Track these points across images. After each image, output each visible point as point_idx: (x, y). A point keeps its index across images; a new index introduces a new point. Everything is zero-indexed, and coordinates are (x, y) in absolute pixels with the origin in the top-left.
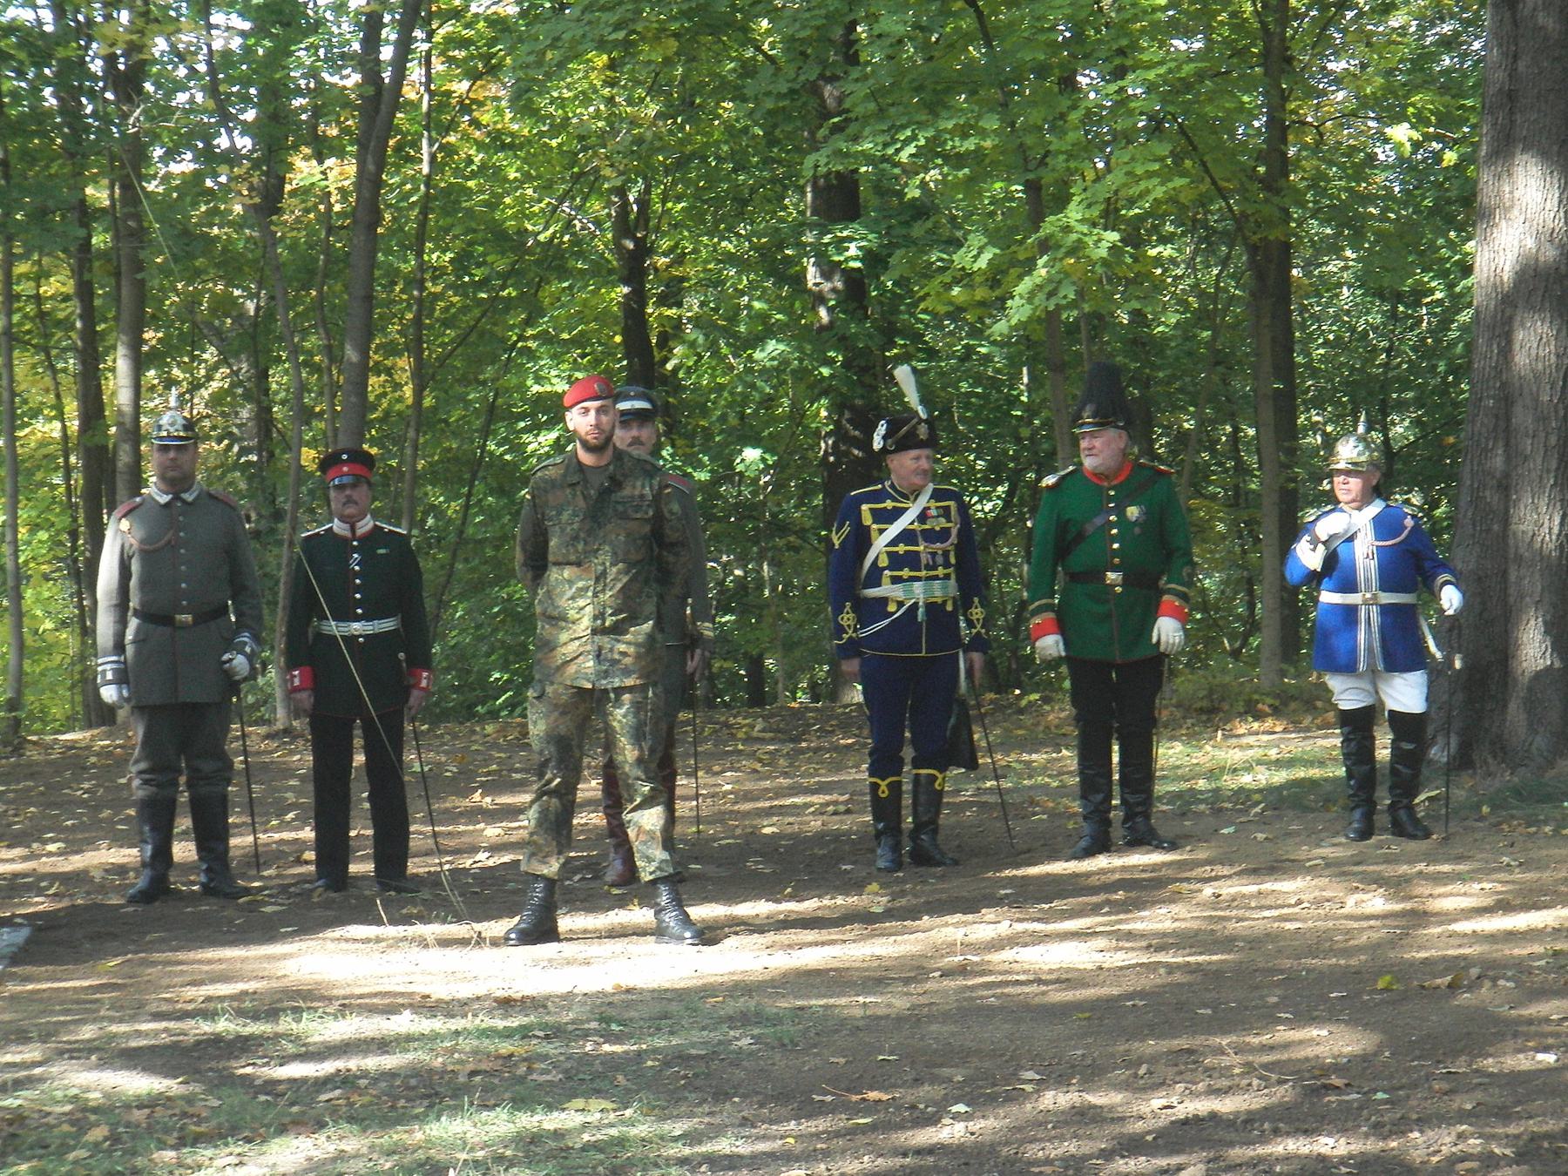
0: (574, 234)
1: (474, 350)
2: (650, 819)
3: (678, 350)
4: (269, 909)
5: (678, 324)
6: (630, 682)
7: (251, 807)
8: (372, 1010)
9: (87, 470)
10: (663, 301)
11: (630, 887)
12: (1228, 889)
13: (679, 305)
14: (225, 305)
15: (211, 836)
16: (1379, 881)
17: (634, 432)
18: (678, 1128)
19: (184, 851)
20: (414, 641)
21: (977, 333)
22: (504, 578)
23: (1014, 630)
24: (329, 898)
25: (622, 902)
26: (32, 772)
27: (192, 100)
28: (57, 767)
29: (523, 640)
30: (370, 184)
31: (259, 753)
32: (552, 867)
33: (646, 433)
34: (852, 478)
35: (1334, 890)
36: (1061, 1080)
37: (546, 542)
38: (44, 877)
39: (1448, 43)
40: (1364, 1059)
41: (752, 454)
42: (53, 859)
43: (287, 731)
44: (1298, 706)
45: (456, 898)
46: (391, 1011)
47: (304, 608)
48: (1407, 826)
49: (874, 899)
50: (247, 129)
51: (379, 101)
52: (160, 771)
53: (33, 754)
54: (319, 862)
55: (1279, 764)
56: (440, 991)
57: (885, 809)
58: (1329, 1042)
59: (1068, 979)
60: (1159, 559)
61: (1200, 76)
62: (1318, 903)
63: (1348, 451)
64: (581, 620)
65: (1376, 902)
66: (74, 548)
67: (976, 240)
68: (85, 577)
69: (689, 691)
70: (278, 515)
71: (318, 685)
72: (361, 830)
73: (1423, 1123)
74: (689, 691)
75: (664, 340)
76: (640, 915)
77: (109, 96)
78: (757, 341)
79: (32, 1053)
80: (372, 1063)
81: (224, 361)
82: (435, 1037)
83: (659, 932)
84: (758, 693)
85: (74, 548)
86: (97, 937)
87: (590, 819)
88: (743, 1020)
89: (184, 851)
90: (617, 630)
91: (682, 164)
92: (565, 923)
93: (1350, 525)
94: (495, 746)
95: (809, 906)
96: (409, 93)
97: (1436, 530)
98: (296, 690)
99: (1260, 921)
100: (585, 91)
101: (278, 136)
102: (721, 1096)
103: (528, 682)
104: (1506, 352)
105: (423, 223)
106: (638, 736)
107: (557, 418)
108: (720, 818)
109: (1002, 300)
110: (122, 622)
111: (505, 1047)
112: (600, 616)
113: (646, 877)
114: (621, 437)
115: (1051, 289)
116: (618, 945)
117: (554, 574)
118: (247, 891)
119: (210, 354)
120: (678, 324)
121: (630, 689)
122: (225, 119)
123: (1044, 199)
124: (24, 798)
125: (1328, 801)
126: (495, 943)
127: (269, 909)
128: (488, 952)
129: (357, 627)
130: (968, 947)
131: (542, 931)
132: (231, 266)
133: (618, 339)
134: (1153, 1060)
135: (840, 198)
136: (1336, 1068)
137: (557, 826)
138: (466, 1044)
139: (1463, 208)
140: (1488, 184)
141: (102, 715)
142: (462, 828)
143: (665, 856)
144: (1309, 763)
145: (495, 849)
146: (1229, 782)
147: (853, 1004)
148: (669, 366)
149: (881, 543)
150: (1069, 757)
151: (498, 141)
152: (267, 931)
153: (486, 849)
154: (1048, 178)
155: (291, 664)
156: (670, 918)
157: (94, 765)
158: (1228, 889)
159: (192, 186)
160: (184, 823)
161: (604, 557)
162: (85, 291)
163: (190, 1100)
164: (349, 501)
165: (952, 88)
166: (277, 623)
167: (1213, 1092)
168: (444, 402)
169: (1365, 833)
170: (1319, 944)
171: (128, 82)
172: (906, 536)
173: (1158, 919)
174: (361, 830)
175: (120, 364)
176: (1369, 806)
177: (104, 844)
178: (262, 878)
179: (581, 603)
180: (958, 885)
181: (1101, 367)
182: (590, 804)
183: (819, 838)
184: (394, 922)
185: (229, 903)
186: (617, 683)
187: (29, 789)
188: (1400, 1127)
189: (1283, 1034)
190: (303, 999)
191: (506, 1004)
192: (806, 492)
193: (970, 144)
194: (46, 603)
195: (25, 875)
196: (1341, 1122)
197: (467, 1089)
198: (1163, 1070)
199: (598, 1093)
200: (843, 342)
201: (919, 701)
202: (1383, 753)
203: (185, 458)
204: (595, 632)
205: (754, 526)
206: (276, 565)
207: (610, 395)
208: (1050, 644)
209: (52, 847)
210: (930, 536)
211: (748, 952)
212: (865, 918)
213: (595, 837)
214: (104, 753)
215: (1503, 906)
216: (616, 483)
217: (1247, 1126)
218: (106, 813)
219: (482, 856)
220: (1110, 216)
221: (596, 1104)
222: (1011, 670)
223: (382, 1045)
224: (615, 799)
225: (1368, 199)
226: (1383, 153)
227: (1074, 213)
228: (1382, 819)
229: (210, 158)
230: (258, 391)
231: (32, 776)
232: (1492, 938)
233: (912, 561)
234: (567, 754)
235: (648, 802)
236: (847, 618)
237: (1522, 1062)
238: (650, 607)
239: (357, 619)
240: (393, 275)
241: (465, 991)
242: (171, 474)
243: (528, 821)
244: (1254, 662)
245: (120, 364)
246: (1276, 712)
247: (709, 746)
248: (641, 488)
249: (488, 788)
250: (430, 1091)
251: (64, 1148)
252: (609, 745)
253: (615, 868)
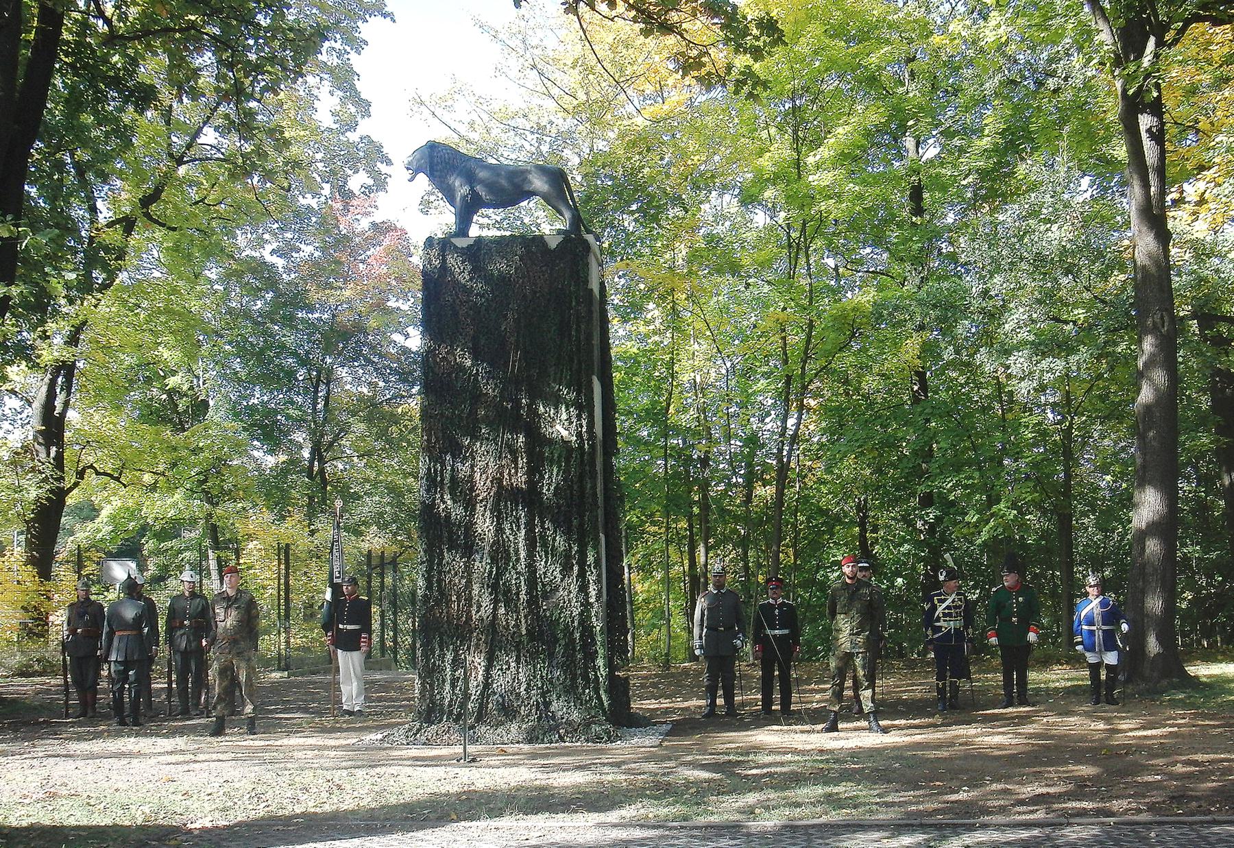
1: (813, 546)
2: (868, 693)
8: (779, 753)
9: (691, 581)
10: (872, 532)
11: (861, 714)
12: (1051, 720)
14: (735, 531)
15: (729, 697)
16: (1102, 718)
18: (876, 792)
19: (720, 701)
21: (971, 543)
22: (823, 616)
23: (981, 634)
24: (766, 717)
26: (673, 675)
29: (828, 638)
30: (780, 493)
32: (836, 708)
33: (867, 574)
34: (932, 585)
35: (1087, 721)
36: (999, 781)
39: (1123, 449)
40: (1098, 776)
41: (900, 580)
44: (1076, 661)
45: (806, 717)
46: (785, 753)
47: (759, 628)
48: (1111, 701)
49: (938, 720)
51: (783, 469)
52: (713, 678)
53: (673, 670)
55: (1068, 680)
56: (800, 747)
57: (941, 691)
58: (1086, 770)
59: (999, 747)
60: (1029, 615)
61: (1043, 460)
62: (1082, 725)
63: (1092, 580)
64: (846, 631)
65: (1102, 726)
67: (972, 512)
68: (690, 616)
69: (880, 654)
70: (751, 597)
71: (763, 650)
72: (777, 696)
73: (1117, 798)
74: (880, 654)
75: (872, 544)
76: (864, 724)
78: (901, 545)
79: (672, 764)
80: (778, 769)
82: (798, 762)
83: (870, 729)
84: (901, 655)
86: (693, 728)
87: (848, 693)
88: (897, 758)
89: (720, 701)
90: (858, 634)
91: (878, 488)
92: (840, 726)
93: (1091, 606)
95: (917, 721)
96: (792, 465)
97: (1120, 606)
99: (1062, 731)
100: (848, 467)
102: (889, 782)
103: (830, 650)
104: (1143, 549)
106: (864, 668)
107: (840, 568)
108: (889, 693)
109: (979, 533)
111: (821, 766)
115: (995, 528)
116: (857, 733)
117: (838, 617)
122: (735, 473)
123: (993, 500)
124: (670, 684)
125: (1085, 692)
128: (816, 735)
130: (967, 737)
131: (833, 728)
132: (737, 519)
134: (1028, 775)
135: (927, 501)
136: (1089, 780)
137: (838, 695)
138: (809, 765)
139: (1127, 502)
140: (1137, 497)
141: (694, 658)
144: (1078, 680)
146: (1052, 685)
147: (932, 754)
149: (940, 610)
150: (1000, 677)
151: (821, 482)
152: (745, 727)
154: (994, 493)
156: (873, 724)
158: (1051, 720)
159: (725, 494)
160: (720, 692)
161: (854, 612)
162: (691, 526)
163: (721, 780)
165: (963, 465)
166: (751, 631)
167: (1047, 785)
168: (805, 561)
169: (1097, 703)
170: (1082, 739)
171: (705, 462)
172: (948, 607)
173: (1029, 729)
174: (777, 696)
175: (701, 549)
176: (1098, 694)
180: (962, 717)
181: (1006, 551)
183: (920, 700)
185: (733, 719)
188: (1111, 798)
189: (1071, 767)
190: (757, 749)
191: (821, 752)
192: (917, 591)
193: (970, 482)
194: (678, 621)
196: (1090, 797)
197: (809, 779)
198: (1031, 778)
199: (850, 780)
200: (928, 545)
201: (952, 658)
202: (1103, 677)
205: (900, 603)
206: (751, 612)
208: (994, 640)
210: (956, 607)
211: (896, 737)
212: (935, 726)
213: (850, 698)
215: (1144, 728)
216: (858, 589)
217: (1059, 797)
220: (1014, 506)
221: (849, 784)
222: (981, 647)
223: (782, 764)
224: (856, 686)
225: (1097, 499)
226: (1103, 484)
227: (1002, 505)
228: (1103, 698)
229: (730, 485)
230: (745, 557)
232: (1140, 738)
233: (950, 615)
234: (841, 673)
236: (929, 632)
237: (1150, 779)
240: (788, 523)
241: (808, 747)
242: (460, 270)
243: (830, 693)
244: (1060, 646)
245: (701, 549)
246: (1067, 663)
250: (796, 779)
251: (683, 795)
252: (855, 670)
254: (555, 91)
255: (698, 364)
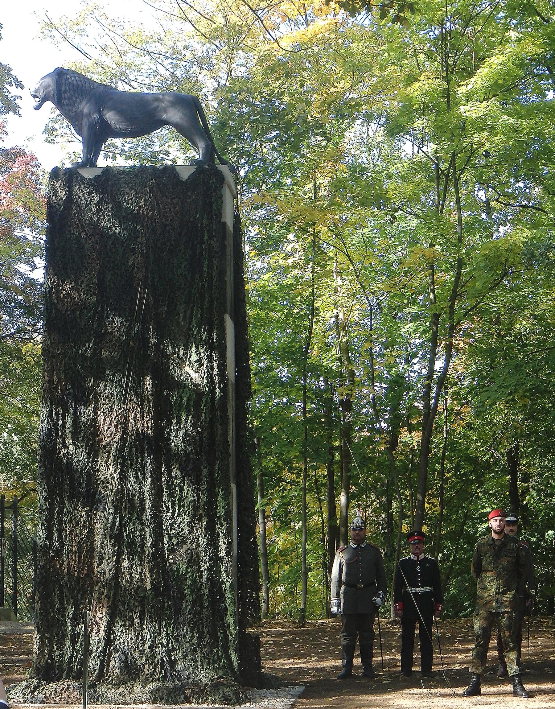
0: (494, 458)
1: (459, 500)
3: (527, 497)
4: (385, 682)
5: (528, 489)
6: (507, 610)
7: (381, 647)
11: (505, 678)
13: (528, 482)
15: (367, 657)
17: (511, 528)
19: (357, 662)
20: (438, 593)
25: (502, 683)
27: (368, 411)
28: (317, 631)
30: (426, 441)
31: (384, 629)
37: (481, 563)
38: (310, 669)
42: (313, 663)
43: (394, 621)
47: (400, 585)
50: (386, 421)
51: (430, 413)
52: (350, 634)
54: (402, 666)
66: (325, 559)
68: (328, 568)
72: (417, 656)
76: (509, 688)
77: (341, 409)
81: (377, 498)
83: (515, 694)
85: (325, 559)
87: (493, 654)
89: (357, 662)
90: (504, 593)
92: (483, 690)
94: (463, 627)
98: (398, 610)
101: (397, 422)
105: (444, 453)
110: (339, 587)
112: (498, 588)
113: (510, 674)
114: (507, 529)
118: (378, 676)
119: (373, 496)
120: (528, 489)
121: (507, 612)
126: (459, 696)
127: (385, 682)
129: (418, 589)
133: (508, 493)
137: (481, 655)
142: (451, 655)
143: (517, 668)
145: (461, 663)
148: (524, 503)
153: (458, 663)
155: (395, 602)
156: (518, 689)
157: (329, 631)
160: (357, 653)
162: (331, 474)
164: (417, 548)
166: (391, 591)
174: (417, 656)
177: (223, 220)
178: (383, 671)
179: (492, 584)
182: (493, 648)
184: (426, 688)
186: (503, 610)
187: (306, 639)
195: (304, 668)
203: (362, 533)
204: (496, 593)
207: (503, 515)
209: (313, 659)
213: (494, 659)
214: (333, 627)
218: (332, 648)
219: (457, 665)
231: (308, 634)
235: (512, 649)
238: (515, 586)
239: (419, 587)
247: (534, 629)
248: (513, 546)
249: (460, 642)
253: (501, 670)
254: (192, 15)
255: (339, 301)
